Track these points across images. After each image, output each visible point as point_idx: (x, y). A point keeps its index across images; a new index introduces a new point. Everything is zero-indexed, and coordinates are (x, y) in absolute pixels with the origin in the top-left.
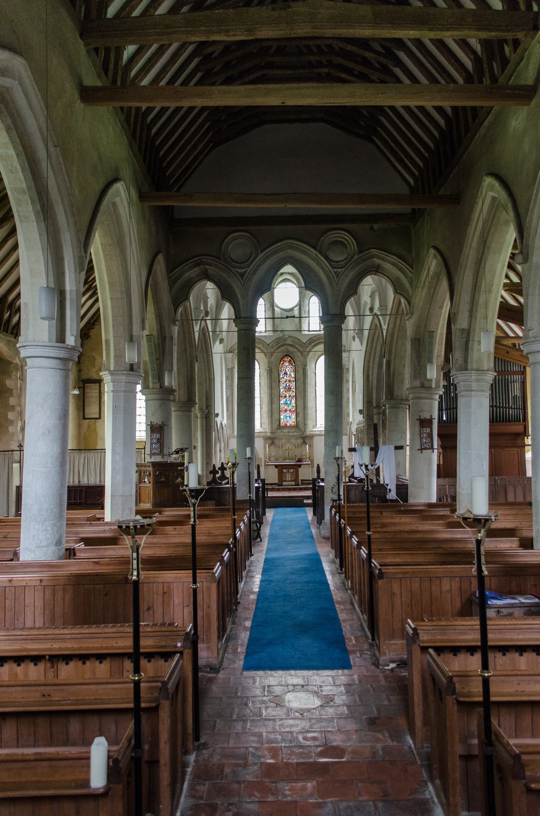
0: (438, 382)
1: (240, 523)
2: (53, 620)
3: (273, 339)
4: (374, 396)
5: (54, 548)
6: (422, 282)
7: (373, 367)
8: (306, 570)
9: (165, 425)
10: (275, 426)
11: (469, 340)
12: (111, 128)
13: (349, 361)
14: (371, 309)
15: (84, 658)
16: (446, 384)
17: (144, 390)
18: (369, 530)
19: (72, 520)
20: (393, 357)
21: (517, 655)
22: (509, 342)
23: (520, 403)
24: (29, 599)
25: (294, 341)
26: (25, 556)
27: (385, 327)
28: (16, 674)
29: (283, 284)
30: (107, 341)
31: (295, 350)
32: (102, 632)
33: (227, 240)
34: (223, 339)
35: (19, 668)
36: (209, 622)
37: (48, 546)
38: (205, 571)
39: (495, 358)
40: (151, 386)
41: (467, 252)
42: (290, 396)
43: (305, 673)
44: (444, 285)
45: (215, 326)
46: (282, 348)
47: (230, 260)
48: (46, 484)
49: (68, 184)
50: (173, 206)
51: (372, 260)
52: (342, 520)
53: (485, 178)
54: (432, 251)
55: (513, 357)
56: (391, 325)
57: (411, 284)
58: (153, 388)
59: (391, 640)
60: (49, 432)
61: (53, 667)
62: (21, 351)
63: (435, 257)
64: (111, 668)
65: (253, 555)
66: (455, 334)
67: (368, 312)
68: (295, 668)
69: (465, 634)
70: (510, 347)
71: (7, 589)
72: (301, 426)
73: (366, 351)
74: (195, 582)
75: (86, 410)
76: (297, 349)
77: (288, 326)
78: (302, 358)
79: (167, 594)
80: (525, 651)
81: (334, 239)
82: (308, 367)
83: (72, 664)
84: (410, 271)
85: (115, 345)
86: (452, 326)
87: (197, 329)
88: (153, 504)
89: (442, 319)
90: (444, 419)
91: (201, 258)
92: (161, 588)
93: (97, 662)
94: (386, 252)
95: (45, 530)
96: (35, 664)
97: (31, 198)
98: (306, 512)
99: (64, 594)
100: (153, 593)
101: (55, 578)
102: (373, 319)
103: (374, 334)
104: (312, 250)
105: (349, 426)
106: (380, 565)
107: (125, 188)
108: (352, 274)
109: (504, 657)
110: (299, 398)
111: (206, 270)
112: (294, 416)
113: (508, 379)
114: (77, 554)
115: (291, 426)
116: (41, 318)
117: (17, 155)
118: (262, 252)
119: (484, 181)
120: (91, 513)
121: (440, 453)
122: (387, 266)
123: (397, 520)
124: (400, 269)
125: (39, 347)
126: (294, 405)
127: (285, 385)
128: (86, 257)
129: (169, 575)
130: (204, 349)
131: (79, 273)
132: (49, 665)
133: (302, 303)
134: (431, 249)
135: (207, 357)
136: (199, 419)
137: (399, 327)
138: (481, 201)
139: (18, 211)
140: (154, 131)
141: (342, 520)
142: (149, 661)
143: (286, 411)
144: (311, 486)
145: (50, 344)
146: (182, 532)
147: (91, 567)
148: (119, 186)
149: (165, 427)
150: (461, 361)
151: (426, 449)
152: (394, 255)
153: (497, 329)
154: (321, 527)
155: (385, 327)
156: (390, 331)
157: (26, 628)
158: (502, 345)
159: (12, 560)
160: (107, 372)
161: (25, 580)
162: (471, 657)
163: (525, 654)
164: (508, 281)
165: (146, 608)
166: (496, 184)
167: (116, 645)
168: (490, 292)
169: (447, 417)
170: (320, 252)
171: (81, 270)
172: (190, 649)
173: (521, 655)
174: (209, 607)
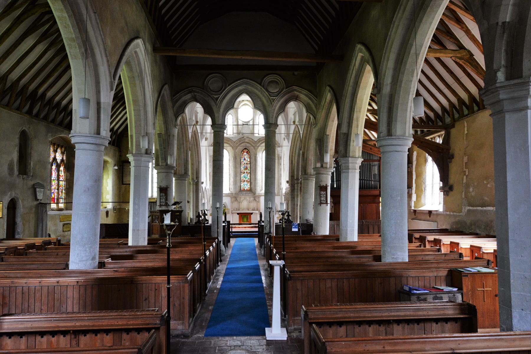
0: (331, 165)
1: (210, 247)
2: (85, 307)
3: (237, 139)
4: (295, 173)
5: (91, 262)
6: (322, 106)
7: (295, 156)
8: (251, 274)
9: (169, 188)
10: (238, 189)
11: (348, 139)
12: (134, 7)
13: (281, 152)
14: (294, 122)
15: (96, 332)
16: (336, 166)
17: (156, 167)
18: (284, 251)
19: (108, 245)
20: (306, 150)
21: (367, 326)
22: (372, 143)
23: (377, 178)
24: (70, 294)
25: (250, 141)
26: (72, 266)
27: (301, 133)
28: (51, 342)
29: (244, 107)
30: (132, 136)
31: (250, 145)
32: (108, 315)
33: (208, 78)
34: (207, 138)
35: (53, 339)
36: (184, 307)
37: (87, 260)
38: (182, 276)
39: (362, 151)
40: (160, 164)
41: (347, 88)
42: (247, 173)
43: (243, 338)
44: (334, 109)
45: (202, 130)
46: (243, 144)
47: (209, 90)
48: (86, 222)
49: (103, 37)
50: (176, 56)
51: (293, 92)
52: (272, 245)
53: (357, 45)
54: (328, 88)
55: (375, 152)
56: (305, 131)
57: (316, 107)
58: (161, 166)
59: (295, 317)
60: (88, 190)
61: (76, 338)
62: (72, 139)
63: (329, 91)
64: (113, 338)
65: (219, 266)
66: (340, 135)
67: (292, 123)
68: (236, 335)
69: (337, 314)
70: (372, 146)
71: (56, 287)
72: (253, 190)
73: (291, 146)
74: (169, 283)
75: (124, 179)
76: (251, 144)
77: (246, 130)
78: (254, 150)
79: (157, 290)
80: (372, 324)
81: (271, 80)
82: (258, 155)
83: (88, 336)
84: (315, 100)
85: (136, 138)
86: (339, 131)
87: (190, 131)
88: (160, 235)
89: (333, 127)
90: (335, 186)
91: (192, 88)
92: (154, 287)
93: (105, 335)
94: (302, 88)
95: (85, 251)
96: (64, 336)
97: (78, 44)
98: (254, 240)
99: (92, 290)
100: (149, 290)
101: (86, 281)
102: (295, 128)
103: (296, 136)
104: (259, 85)
105: (281, 191)
106: (290, 272)
107: (143, 43)
108: (282, 101)
109: (360, 328)
110: (252, 174)
111: (195, 96)
112: (249, 184)
113: (371, 164)
114: (106, 266)
115: (247, 190)
116: (80, 117)
117: (69, 16)
118: (229, 86)
119: (357, 47)
120: (121, 241)
121: (332, 206)
122: (302, 96)
123: (304, 245)
124: (310, 99)
125: (83, 137)
126: (249, 178)
127: (244, 166)
128: (114, 82)
129: (159, 279)
130: (195, 143)
131: (110, 92)
132: (73, 336)
133: (255, 118)
134: (327, 87)
135: (197, 148)
136: (191, 185)
137: (310, 133)
138: (354, 60)
139: (70, 52)
140: (163, 11)
141: (272, 245)
142: (139, 334)
143: (244, 181)
144: (257, 225)
145: (89, 135)
146: (174, 252)
147: (112, 274)
148: (139, 41)
149: (169, 189)
150: (343, 152)
151: (323, 203)
152: (306, 89)
153: (364, 134)
154: (262, 249)
155: (301, 133)
156: (304, 135)
157: (75, 313)
158: (368, 144)
159: (65, 269)
160: (131, 155)
161: (68, 282)
162: (340, 328)
163: (372, 326)
164: (372, 108)
165: (144, 299)
166: (363, 48)
167: (117, 323)
168: (360, 112)
169: (336, 185)
170: (263, 87)
171: (112, 90)
172: (164, 326)
173: (370, 326)
174: (184, 298)
